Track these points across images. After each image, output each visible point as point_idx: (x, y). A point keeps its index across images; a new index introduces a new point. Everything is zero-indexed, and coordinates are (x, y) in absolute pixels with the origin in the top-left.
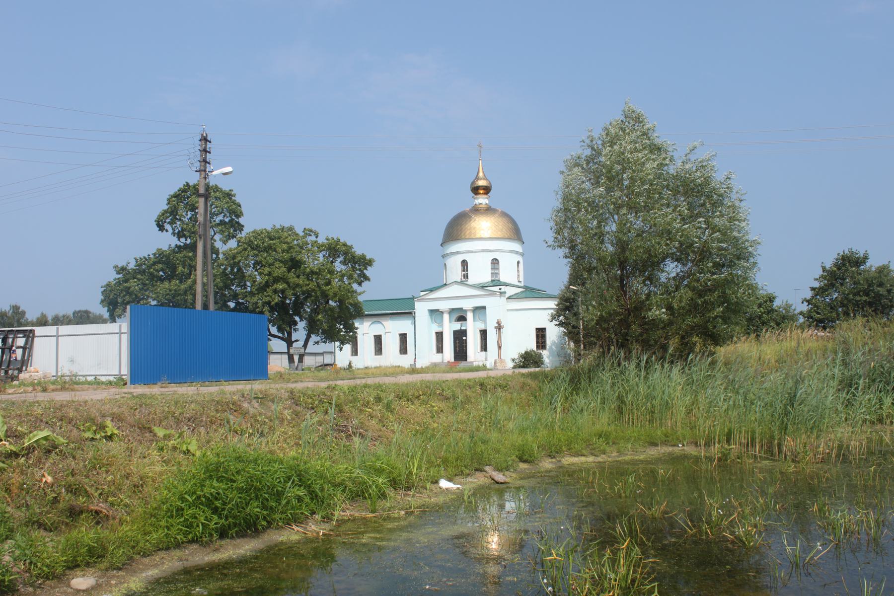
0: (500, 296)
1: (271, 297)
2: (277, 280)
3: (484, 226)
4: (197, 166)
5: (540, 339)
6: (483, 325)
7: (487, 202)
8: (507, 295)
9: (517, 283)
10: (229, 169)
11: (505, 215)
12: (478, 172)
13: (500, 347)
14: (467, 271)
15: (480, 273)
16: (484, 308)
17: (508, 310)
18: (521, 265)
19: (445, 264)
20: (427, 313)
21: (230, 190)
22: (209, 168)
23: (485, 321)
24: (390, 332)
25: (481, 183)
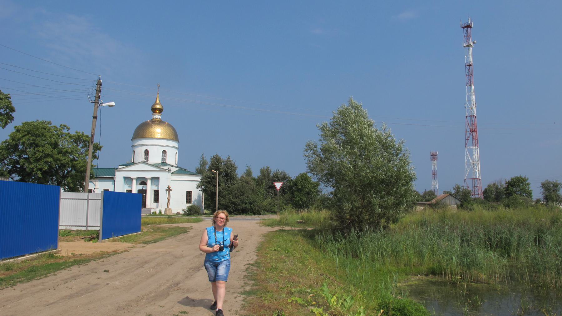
0: (168, 172)
1: (43, 166)
2: (48, 155)
3: (158, 131)
4: (93, 99)
5: (188, 197)
6: (156, 188)
7: (160, 118)
8: (172, 172)
9: (175, 165)
10: (113, 104)
11: (169, 125)
12: (156, 100)
13: (169, 201)
14: (148, 156)
15: (155, 158)
16: (158, 178)
17: (171, 180)
18: (177, 155)
19: (134, 152)
20: (123, 179)
21: (8, 94)
22: (101, 101)
23: (158, 185)
24: (98, 188)
25: (158, 106)
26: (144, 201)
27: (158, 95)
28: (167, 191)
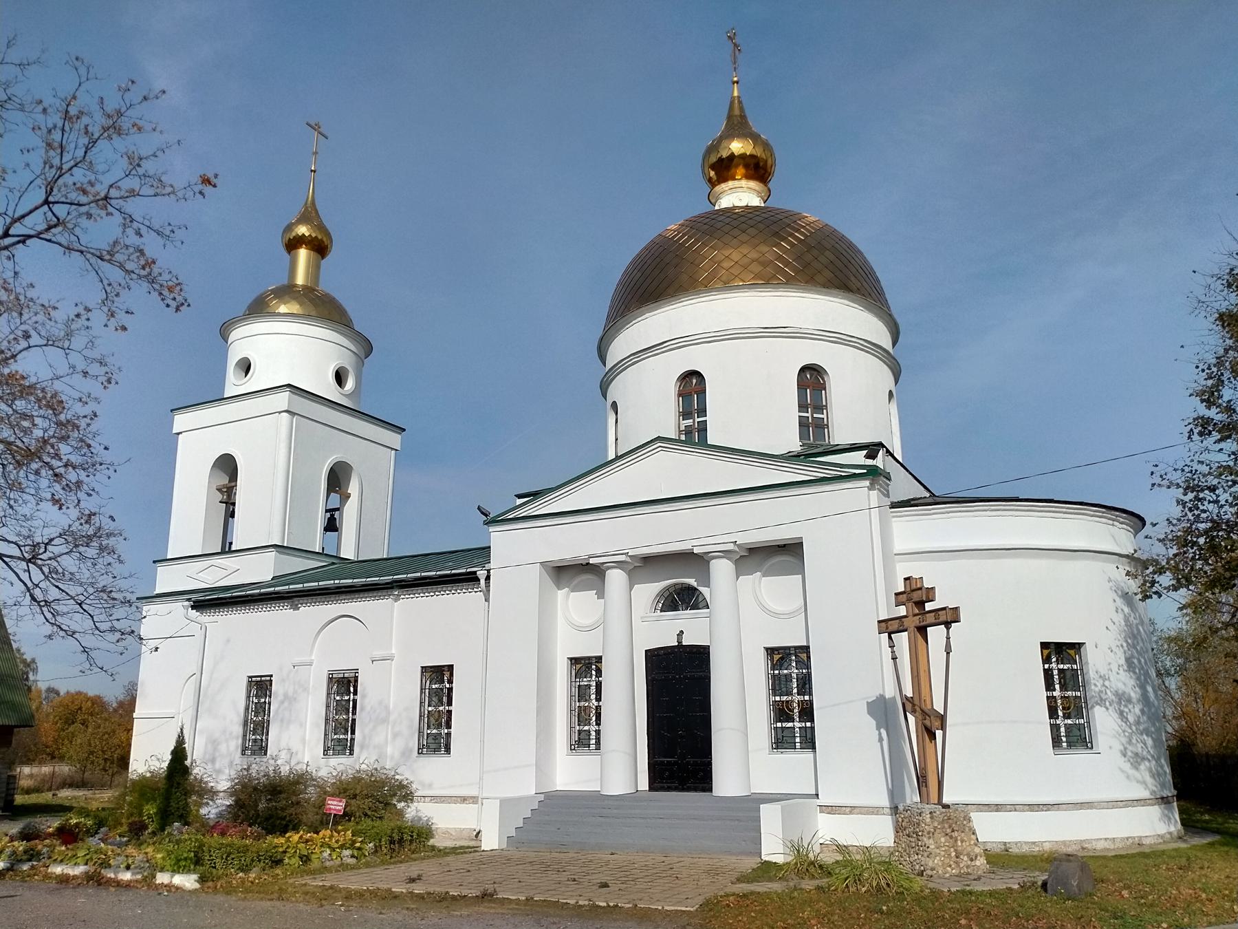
28: (902, 639)
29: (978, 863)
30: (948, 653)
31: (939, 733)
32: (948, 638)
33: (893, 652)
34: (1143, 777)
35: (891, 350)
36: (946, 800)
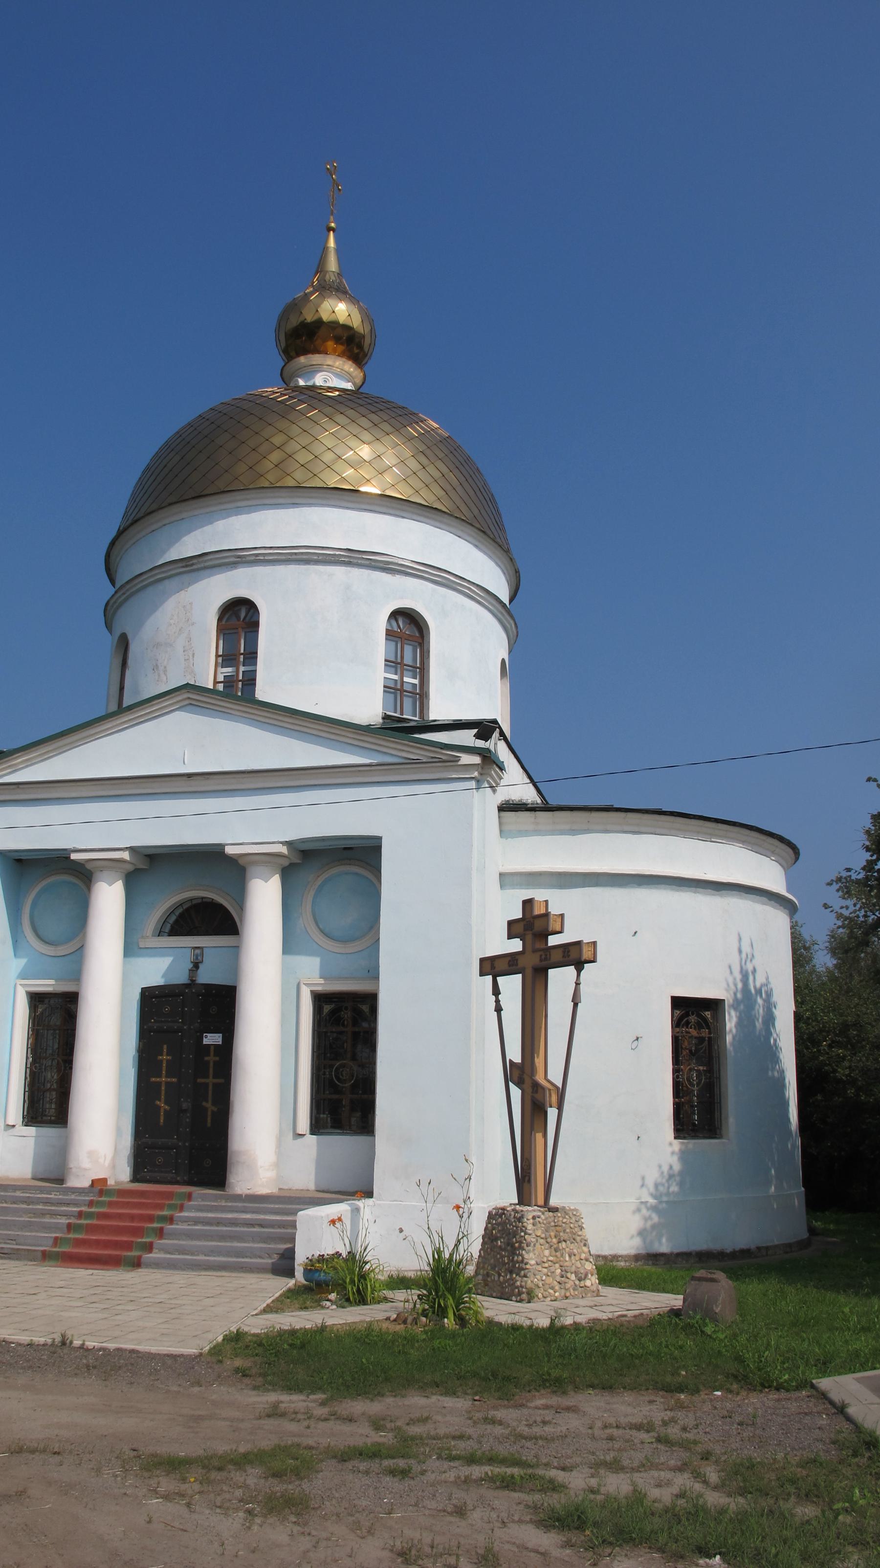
26: (209, 1105)
27: (332, 243)
29: (588, 1283)
30: (576, 1005)
31: (552, 1113)
32: (578, 984)
33: (497, 1001)
34: (530, 1408)
35: (508, 604)
36: (553, 1201)
